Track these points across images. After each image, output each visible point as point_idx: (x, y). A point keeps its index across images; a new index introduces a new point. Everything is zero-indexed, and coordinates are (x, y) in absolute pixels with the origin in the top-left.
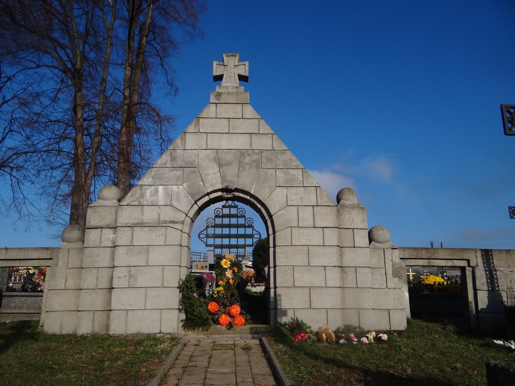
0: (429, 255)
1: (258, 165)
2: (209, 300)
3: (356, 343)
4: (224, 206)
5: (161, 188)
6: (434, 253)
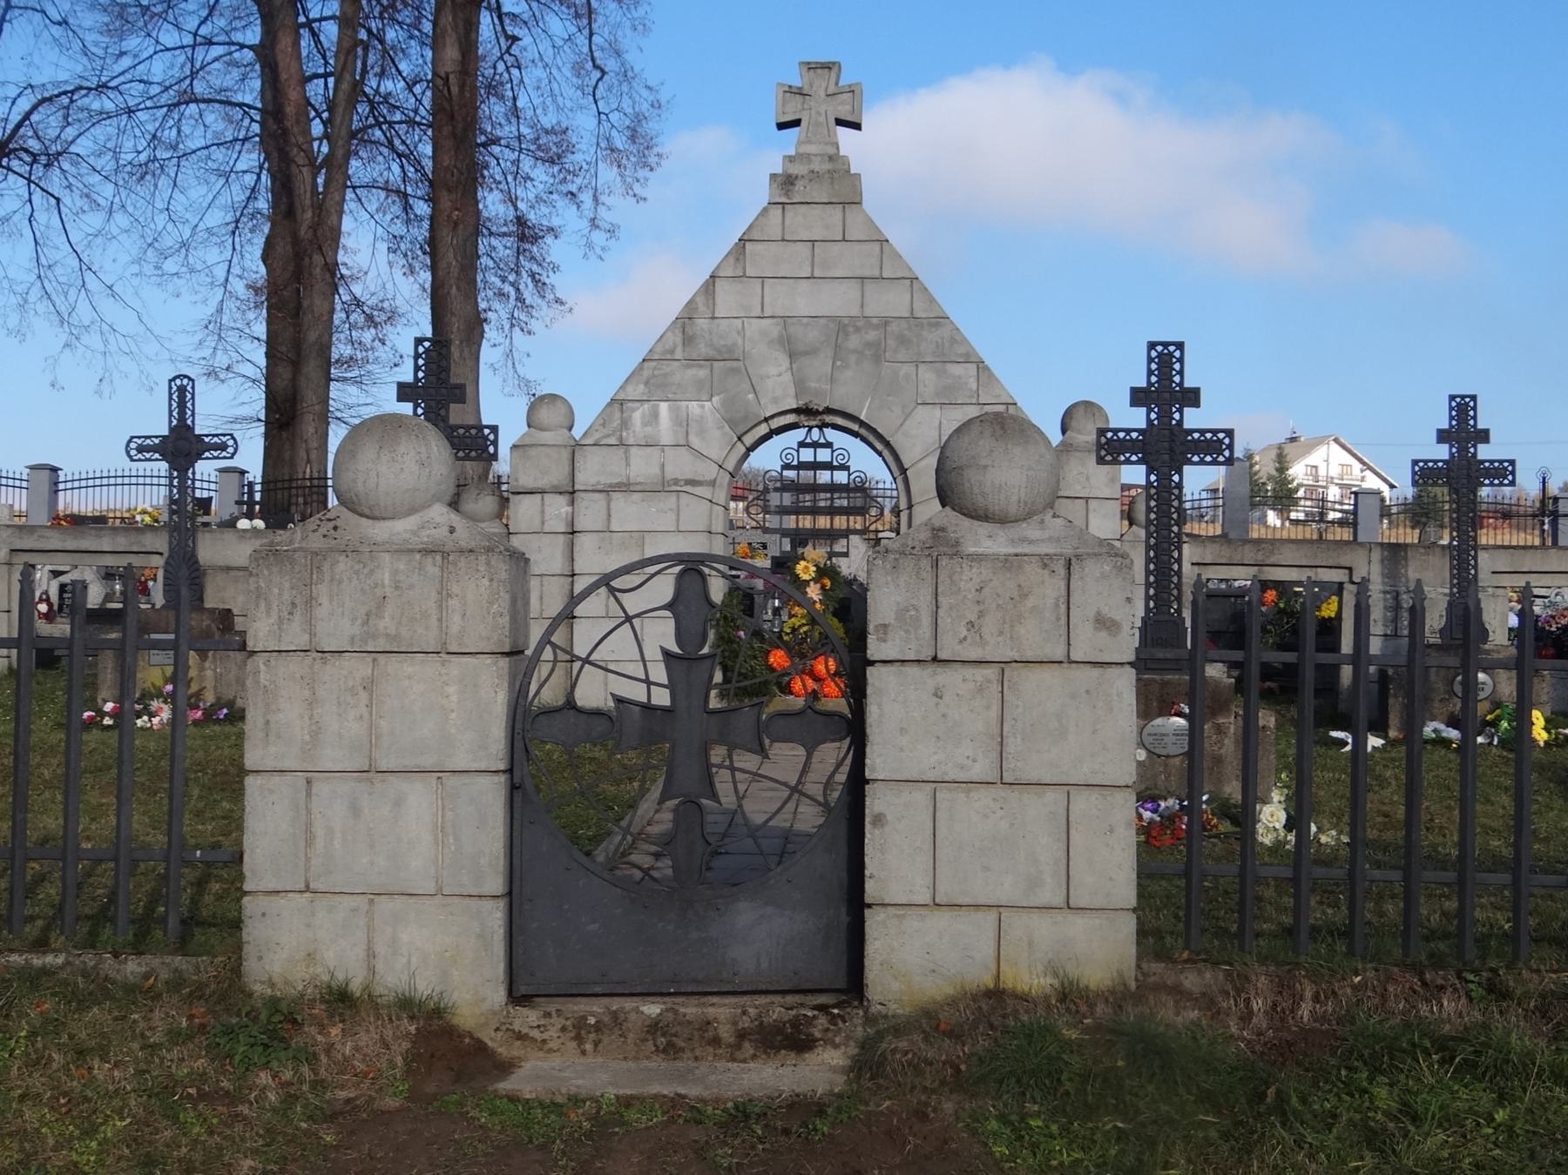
0: (1260, 557)
1: (877, 353)
2: (771, 644)
3: (831, 662)
4: (802, 444)
5: (664, 407)
6: (1272, 552)
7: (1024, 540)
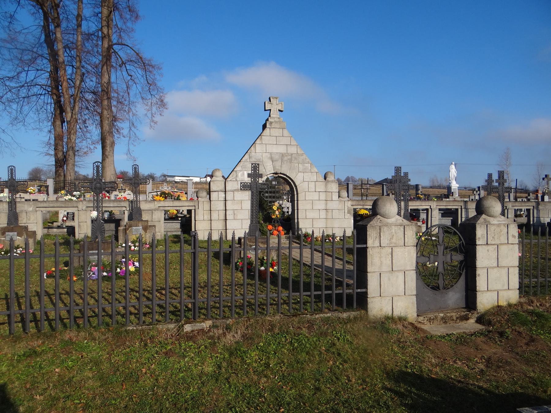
7: (499, 221)
